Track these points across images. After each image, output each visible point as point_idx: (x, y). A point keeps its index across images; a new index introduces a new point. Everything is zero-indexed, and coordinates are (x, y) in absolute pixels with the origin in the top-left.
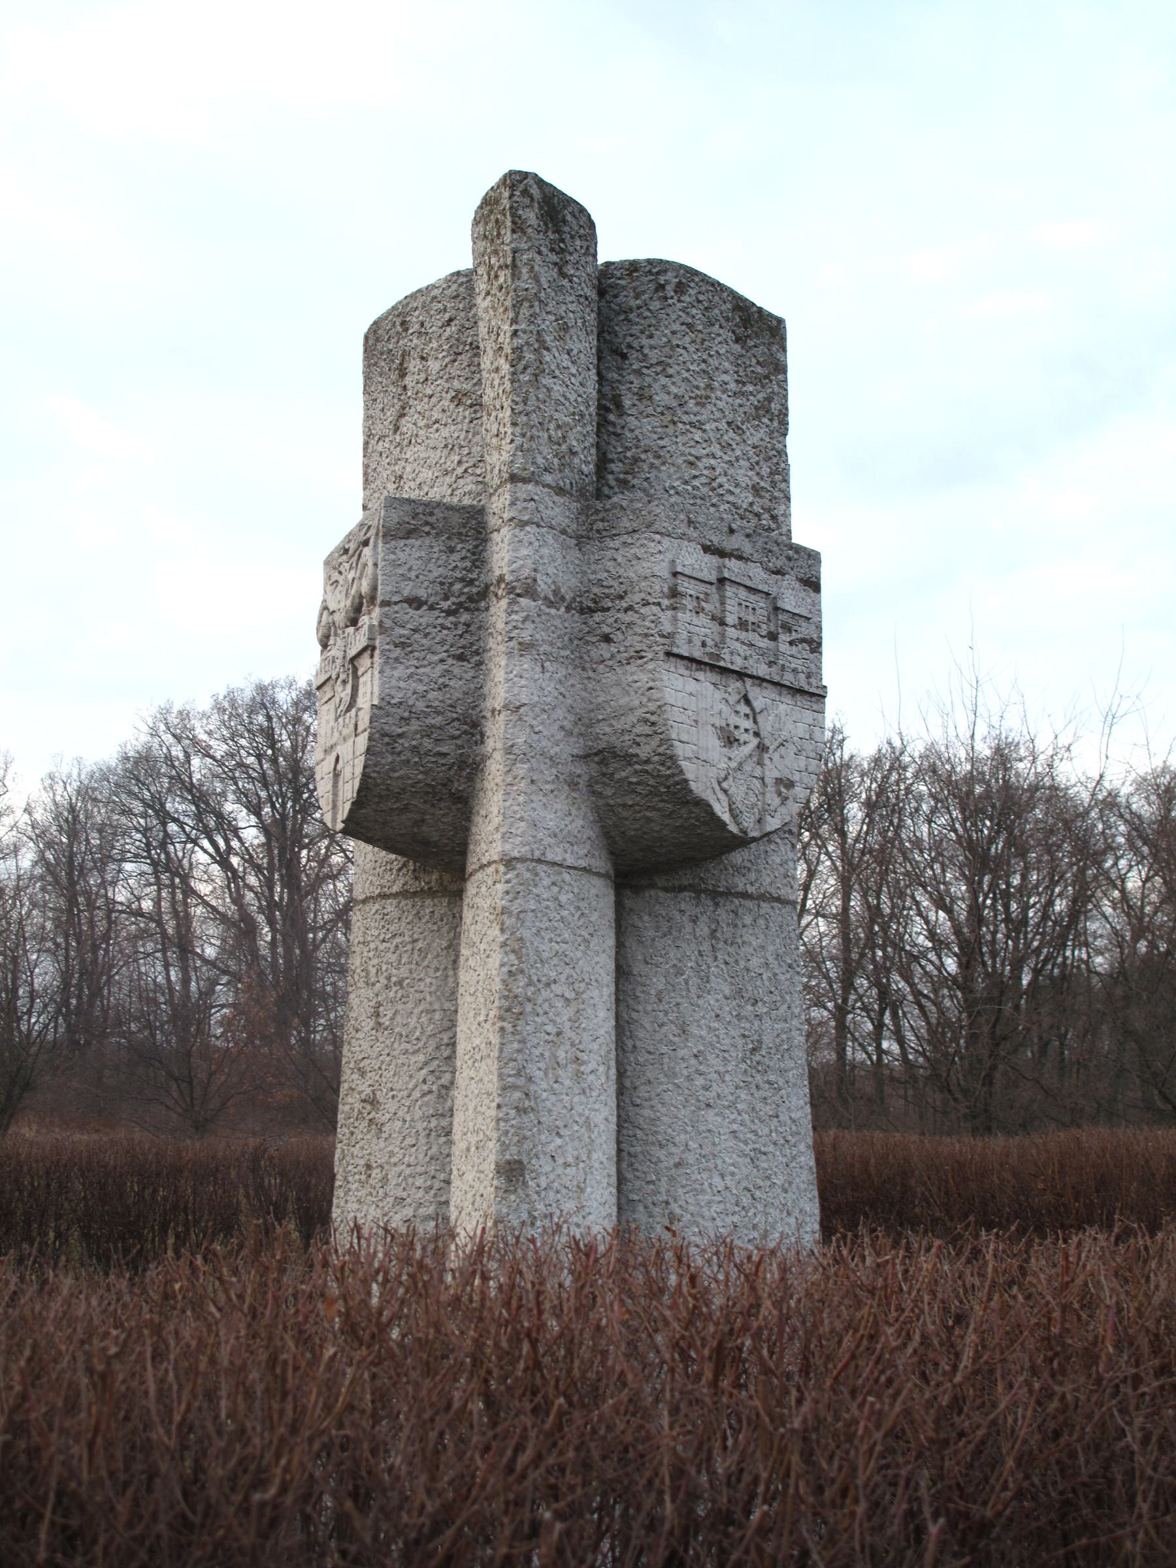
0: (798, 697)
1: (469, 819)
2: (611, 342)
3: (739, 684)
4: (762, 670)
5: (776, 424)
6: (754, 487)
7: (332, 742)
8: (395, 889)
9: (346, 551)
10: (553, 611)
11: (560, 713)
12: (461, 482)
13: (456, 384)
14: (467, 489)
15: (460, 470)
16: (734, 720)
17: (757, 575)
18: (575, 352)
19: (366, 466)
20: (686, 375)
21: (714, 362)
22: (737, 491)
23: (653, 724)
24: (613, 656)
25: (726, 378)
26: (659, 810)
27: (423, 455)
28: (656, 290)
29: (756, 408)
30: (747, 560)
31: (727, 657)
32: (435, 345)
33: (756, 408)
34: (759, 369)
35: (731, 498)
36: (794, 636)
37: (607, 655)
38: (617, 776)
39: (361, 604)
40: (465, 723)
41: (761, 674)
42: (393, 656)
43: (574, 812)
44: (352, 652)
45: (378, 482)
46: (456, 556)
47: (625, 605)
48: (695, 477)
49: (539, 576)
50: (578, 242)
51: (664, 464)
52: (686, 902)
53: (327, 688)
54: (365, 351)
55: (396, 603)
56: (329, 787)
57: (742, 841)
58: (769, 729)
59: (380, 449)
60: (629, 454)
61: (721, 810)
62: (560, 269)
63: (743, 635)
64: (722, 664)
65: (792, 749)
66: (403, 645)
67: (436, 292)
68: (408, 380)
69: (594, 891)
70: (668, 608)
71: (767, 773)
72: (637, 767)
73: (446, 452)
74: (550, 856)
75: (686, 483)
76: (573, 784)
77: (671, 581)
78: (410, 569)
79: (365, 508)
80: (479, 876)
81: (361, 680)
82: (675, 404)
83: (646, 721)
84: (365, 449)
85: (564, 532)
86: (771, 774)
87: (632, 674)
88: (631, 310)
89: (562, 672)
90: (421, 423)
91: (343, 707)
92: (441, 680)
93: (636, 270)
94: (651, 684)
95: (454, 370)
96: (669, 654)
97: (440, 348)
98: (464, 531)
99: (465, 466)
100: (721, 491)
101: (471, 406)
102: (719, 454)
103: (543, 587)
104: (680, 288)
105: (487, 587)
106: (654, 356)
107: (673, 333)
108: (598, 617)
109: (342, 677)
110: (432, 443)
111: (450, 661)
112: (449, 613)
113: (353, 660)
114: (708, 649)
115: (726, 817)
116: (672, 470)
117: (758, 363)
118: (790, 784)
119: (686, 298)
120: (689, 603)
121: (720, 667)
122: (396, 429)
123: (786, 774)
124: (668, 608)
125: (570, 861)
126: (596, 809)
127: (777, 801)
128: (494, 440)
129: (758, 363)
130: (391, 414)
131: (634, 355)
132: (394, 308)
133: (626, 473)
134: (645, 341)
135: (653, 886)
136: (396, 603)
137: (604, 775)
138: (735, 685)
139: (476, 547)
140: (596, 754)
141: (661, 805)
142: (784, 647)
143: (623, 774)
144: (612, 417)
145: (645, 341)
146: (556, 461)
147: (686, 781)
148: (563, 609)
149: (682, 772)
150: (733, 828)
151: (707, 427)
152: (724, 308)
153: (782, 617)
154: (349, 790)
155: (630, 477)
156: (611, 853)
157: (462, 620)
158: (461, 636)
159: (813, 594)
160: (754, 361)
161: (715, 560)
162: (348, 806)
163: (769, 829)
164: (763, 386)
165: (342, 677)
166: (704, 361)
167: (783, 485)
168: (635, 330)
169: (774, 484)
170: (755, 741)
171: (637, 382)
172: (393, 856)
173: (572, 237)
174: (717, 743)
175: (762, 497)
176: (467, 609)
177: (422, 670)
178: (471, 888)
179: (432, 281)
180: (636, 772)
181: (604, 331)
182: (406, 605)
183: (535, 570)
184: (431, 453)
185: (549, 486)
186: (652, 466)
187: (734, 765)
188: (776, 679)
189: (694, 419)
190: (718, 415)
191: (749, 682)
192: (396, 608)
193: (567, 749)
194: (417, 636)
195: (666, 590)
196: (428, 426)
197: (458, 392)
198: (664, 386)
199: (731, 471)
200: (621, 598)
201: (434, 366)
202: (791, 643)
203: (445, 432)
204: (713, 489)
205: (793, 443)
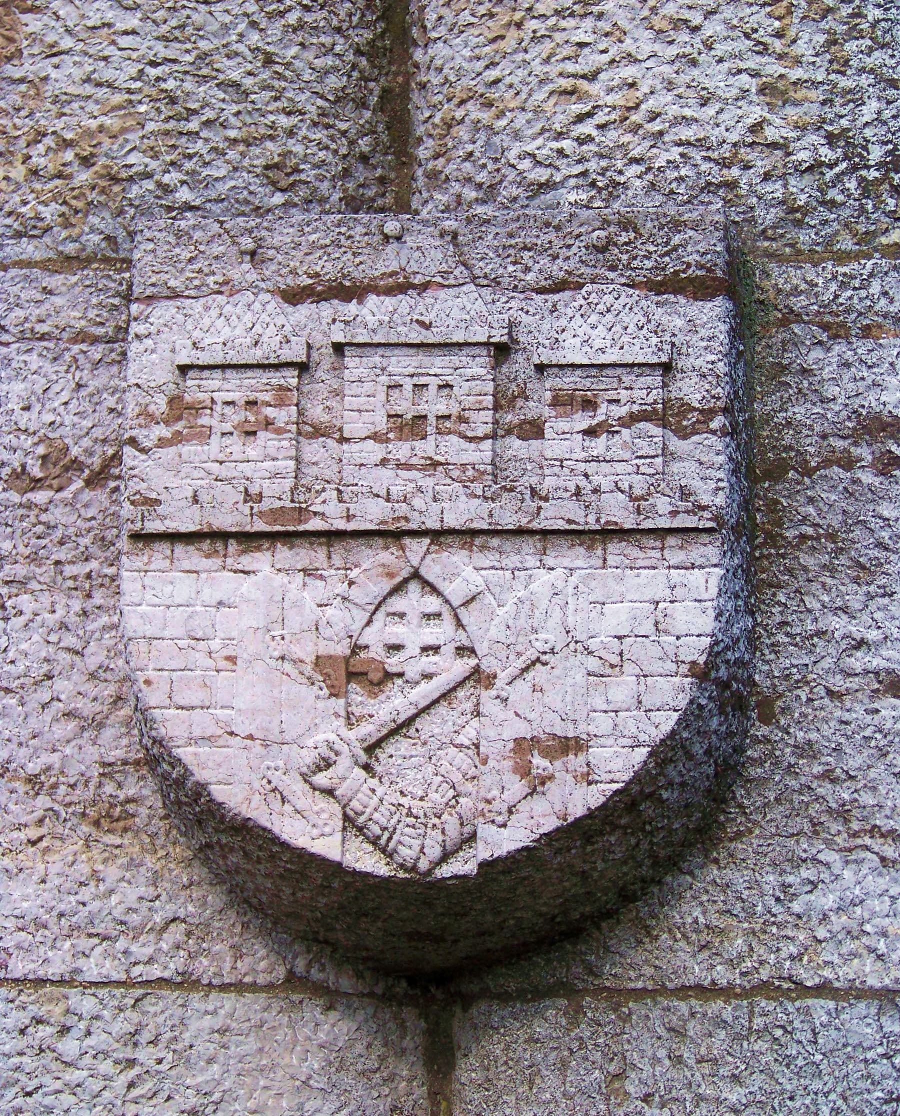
0: (613, 547)
4: (462, 511)
30: (425, 287)
35: (687, 133)
48: (580, 118)
51: (501, 115)
52: (548, 1021)
64: (315, 524)
75: (559, 136)
96: (142, 538)
115: (329, 845)
116: (521, 120)
125: (92, 969)
135: (485, 993)
150: (366, 860)
204: (635, 129)
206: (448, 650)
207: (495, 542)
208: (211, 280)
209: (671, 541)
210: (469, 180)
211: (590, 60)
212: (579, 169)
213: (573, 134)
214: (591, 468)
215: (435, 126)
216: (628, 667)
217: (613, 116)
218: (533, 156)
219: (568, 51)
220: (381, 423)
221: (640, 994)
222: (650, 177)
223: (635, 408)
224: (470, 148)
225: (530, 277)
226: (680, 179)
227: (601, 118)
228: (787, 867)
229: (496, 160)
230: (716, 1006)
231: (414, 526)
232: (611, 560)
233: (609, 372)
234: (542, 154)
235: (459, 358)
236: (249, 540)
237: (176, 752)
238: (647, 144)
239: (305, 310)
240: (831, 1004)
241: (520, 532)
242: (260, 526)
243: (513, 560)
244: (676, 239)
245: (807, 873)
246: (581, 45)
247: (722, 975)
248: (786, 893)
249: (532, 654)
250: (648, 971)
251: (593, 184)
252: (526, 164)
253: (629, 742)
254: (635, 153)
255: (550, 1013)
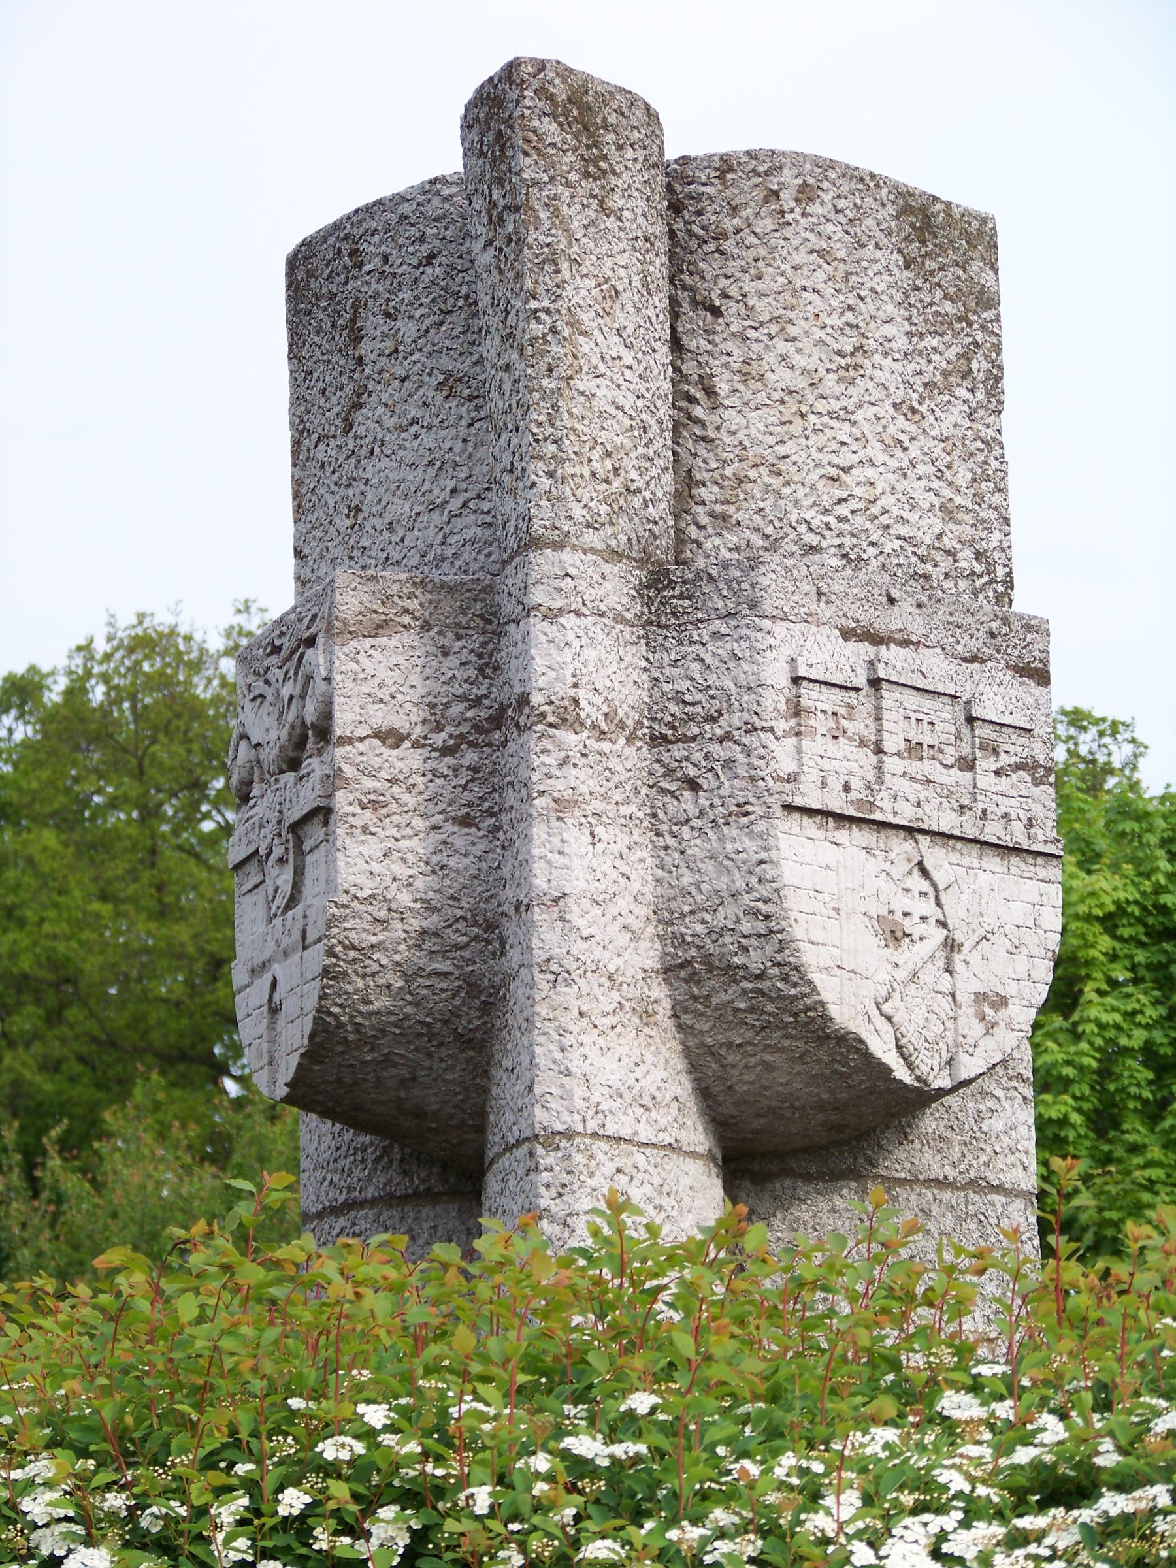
0: (1014, 860)
1: (486, 1074)
2: (693, 290)
3: (909, 846)
4: (948, 821)
5: (980, 395)
6: (943, 507)
7: (265, 957)
8: (370, 1192)
9: (277, 650)
10: (606, 746)
11: (624, 903)
12: (458, 523)
13: (445, 362)
14: (468, 534)
15: (455, 504)
16: (901, 903)
17: (936, 668)
18: (630, 330)
19: (297, 483)
20: (819, 334)
21: (867, 308)
22: (913, 517)
23: (767, 917)
24: (702, 814)
25: (889, 330)
26: (783, 1050)
27: (393, 476)
28: (766, 201)
29: (945, 374)
31: (887, 805)
32: (406, 295)
33: (945, 374)
34: (948, 307)
35: (904, 530)
36: (1004, 760)
37: (693, 811)
38: (715, 1000)
39: (304, 739)
40: (476, 924)
41: (944, 828)
42: (358, 822)
43: (649, 1058)
44: (295, 815)
45: (319, 513)
46: (453, 661)
47: (719, 732)
48: (840, 501)
49: (582, 694)
50: (630, 154)
53: (253, 867)
54: (289, 286)
55: (361, 739)
56: (262, 1028)
57: (922, 1098)
58: (962, 913)
59: (321, 456)
60: (728, 472)
61: (883, 1049)
62: (602, 202)
63: (914, 767)
64: (878, 816)
65: (1001, 944)
66: (375, 805)
67: (406, 208)
68: (364, 348)
69: (685, 1181)
70: (786, 734)
71: (960, 985)
72: (746, 985)
73: (431, 472)
74: (611, 1130)
75: (826, 511)
76: (647, 1015)
77: (789, 690)
78: (381, 685)
79: (298, 553)
80: (506, 1161)
81: (309, 859)
82: (802, 383)
83: (756, 913)
84: (295, 453)
85: (619, 619)
86: (967, 985)
87: (733, 840)
88: (724, 235)
89: (624, 840)
90: (390, 423)
91: (280, 901)
92: (435, 859)
93: (731, 170)
94: (763, 855)
95: (438, 338)
96: (789, 808)
97: (416, 302)
98: (464, 621)
99: (464, 496)
100: (885, 519)
101: (470, 398)
102: (880, 458)
103: (591, 711)
104: (806, 194)
105: (503, 709)
106: (764, 308)
107: (796, 268)
108: (678, 751)
109: (278, 851)
110: (409, 457)
111: (449, 827)
112: (445, 751)
113: (295, 827)
114: (853, 795)
115: (891, 1058)
116: (801, 492)
117: (946, 296)
118: (1001, 1002)
119: (816, 209)
120: (821, 724)
121: (874, 822)
122: (348, 427)
123: (991, 985)
124: (786, 734)
126: (687, 1052)
127: (979, 1029)
128: (506, 477)
129: (946, 296)
130: (337, 403)
131: (732, 309)
132: (337, 226)
133: (727, 502)
134: (749, 286)
136: (361, 739)
137: (695, 998)
138: (901, 847)
139: (484, 645)
140: (682, 966)
141: (786, 1043)
142: (986, 781)
143: (725, 997)
144: (698, 412)
145: (749, 286)
146: (604, 509)
147: (822, 1003)
148: (622, 741)
149: (814, 990)
150: (902, 1074)
151: (859, 416)
152: (883, 214)
153: (983, 731)
154: (295, 1035)
155: (731, 509)
156: (713, 1120)
157: (465, 762)
158: (465, 787)
159: (1039, 691)
160: (939, 294)
161: (866, 650)
162: (295, 1059)
163: (964, 1075)
164: (956, 334)
165: (278, 851)
166: (850, 308)
167: (997, 498)
168: (733, 267)
169: (978, 498)
170: (941, 934)
171: (738, 352)
172: (368, 1139)
173: (620, 148)
174: (878, 941)
175: (957, 522)
176: (472, 744)
177: (404, 844)
178: (493, 1184)
179: (399, 187)
180: (744, 992)
181: (679, 266)
182: (376, 742)
183: (575, 685)
184: (408, 474)
185: (593, 551)
186: (767, 488)
187: (902, 975)
188: (971, 832)
189: (835, 405)
190: (877, 394)
191: (924, 841)
192: (361, 747)
193: (648, 955)
194: (396, 790)
195: (782, 706)
196: (400, 428)
197: (448, 374)
198: (784, 358)
199: (902, 485)
200: (711, 719)
201: (408, 330)
202: (997, 773)
203: (429, 440)
205: (1015, 425)
206: (932, 921)
207: (959, 845)
208: (802, 610)
209: (1040, 861)
210: (758, 530)
211: (846, 458)
212: (837, 542)
213: (836, 513)
214: (999, 799)
215: (723, 477)
216: (1023, 949)
217: (860, 506)
218: (809, 524)
219: (835, 446)
220: (902, 746)
221: (902, 1182)
222: (881, 558)
223: (1018, 760)
224: (761, 505)
225: (960, 648)
226: (899, 565)
227: (853, 504)
228: (978, 1097)
229: (781, 519)
230: (947, 1195)
231: (925, 826)
232: (1013, 870)
233: (1005, 729)
234: (815, 523)
235: (937, 703)
236: (841, 819)
237: (810, 976)
238: (880, 532)
239: (851, 645)
240: (1004, 1200)
241: (975, 841)
242: (851, 812)
243: (967, 861)
244: (1029, 637)
245: (990, 1103)
246: (843, 443)
247: (951, 1173)
248: (979, 1116)
249: (981, 932)
250: (908, 1166)
251: (845, 556)
252: (802, 528)
253: (1026, 1003)
254: (873, 538)
255: (845, 1191)
